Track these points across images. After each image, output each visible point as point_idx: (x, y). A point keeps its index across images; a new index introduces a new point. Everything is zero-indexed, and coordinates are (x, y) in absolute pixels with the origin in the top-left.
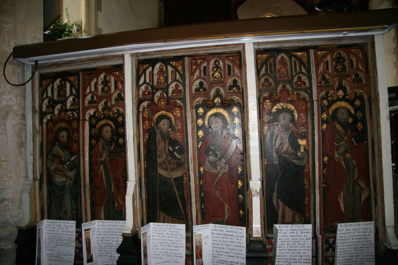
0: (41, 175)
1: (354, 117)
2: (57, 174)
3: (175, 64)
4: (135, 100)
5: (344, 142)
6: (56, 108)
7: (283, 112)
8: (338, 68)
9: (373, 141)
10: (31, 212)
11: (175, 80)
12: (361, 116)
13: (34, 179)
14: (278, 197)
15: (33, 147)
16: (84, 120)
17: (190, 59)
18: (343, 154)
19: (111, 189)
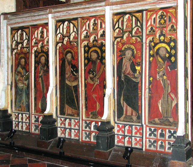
0: (12, 83)
1: (169, 53)
3: (74, 22)
4: (54, 43)
5: (163, 69)
6: (19, 46)
7: (128, 50)
8: (161, 22)
10: (5, 101)
11: (137, 25)
12: (174, 52)
13: (7, 84)
15: (7, 67)
16: (32, 53)
18: (162, 76)
19: (44, 91)
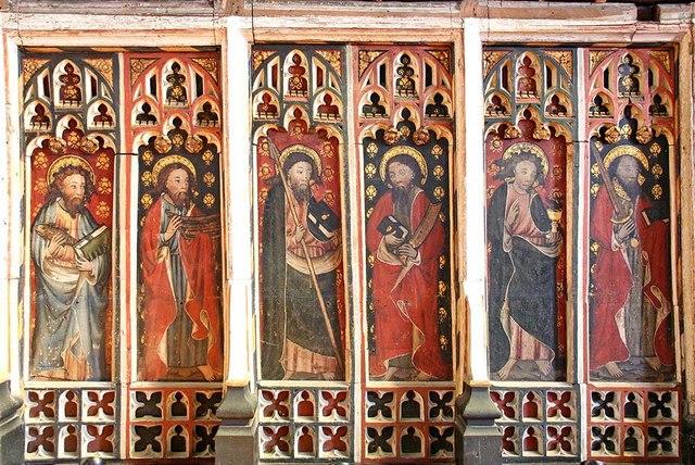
2: (57, 266)
9: (679, 218)
14: (510, 313)
17: (357, 48)
19: (184, 298)
